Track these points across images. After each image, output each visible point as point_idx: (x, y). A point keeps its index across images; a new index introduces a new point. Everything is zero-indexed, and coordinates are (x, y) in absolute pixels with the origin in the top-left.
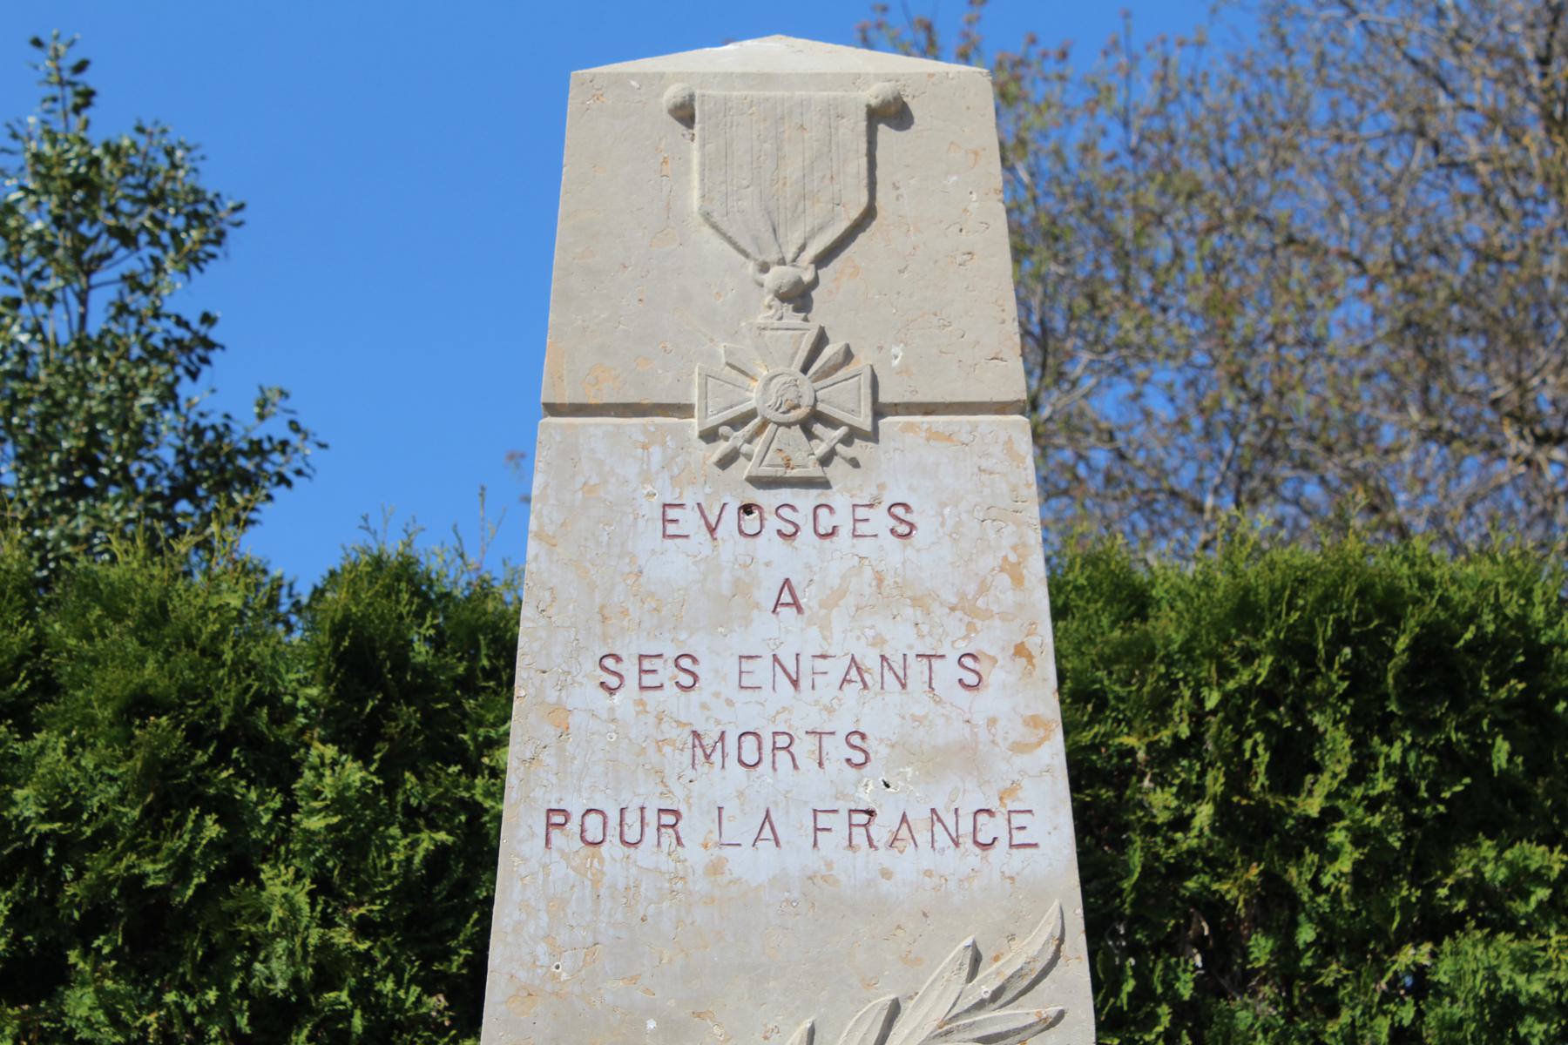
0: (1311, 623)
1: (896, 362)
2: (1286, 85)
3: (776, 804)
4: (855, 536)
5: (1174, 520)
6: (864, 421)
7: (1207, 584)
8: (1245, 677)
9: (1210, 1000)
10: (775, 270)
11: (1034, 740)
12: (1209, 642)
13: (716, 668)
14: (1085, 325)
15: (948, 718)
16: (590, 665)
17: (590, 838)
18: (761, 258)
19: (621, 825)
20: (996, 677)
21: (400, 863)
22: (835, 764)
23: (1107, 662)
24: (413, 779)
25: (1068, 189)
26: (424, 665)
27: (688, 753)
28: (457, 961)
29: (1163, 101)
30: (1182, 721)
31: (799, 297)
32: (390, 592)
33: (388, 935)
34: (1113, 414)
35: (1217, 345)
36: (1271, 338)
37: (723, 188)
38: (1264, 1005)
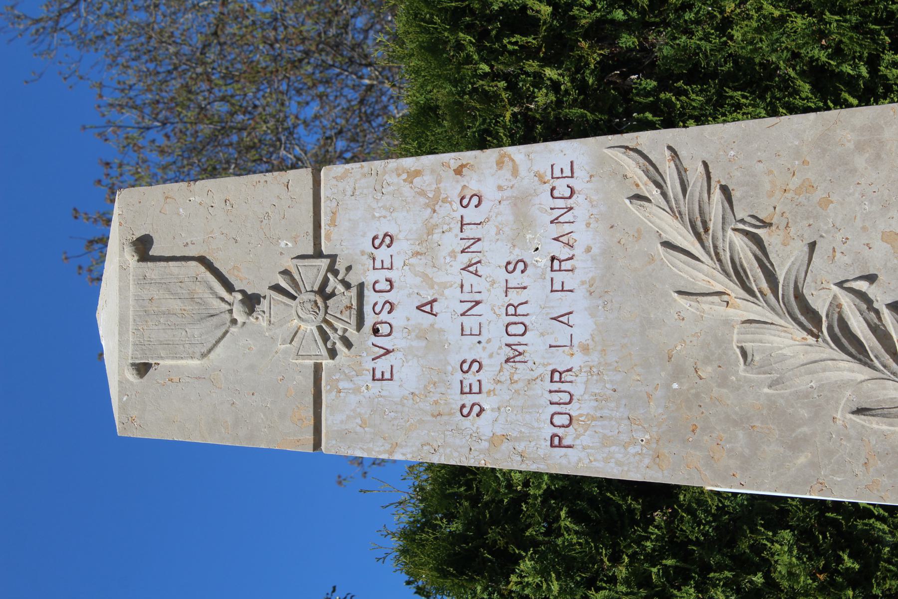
0: (440, 10)
1: (290, 245)
2: (123, 35)
3: (548, 314)
4: (391, 269)
5: (377, 102)
6: (324, 263)
7: (417, 72)
8: (471, 49)
9: (657, 70)
10: (235, 316)
11: (510, 164)
12: (451, 69)
13: (468, 350)
14: (264, 152)
15: (497, 214)
16: (466, 423)
17: (567, 422)
18: (228, 324)
19: (560, 404)
20: (474, 186)
21: (578, 538)
22: (524, 280)
23: (463, 129)
24: (530, 530)
25: (185, 162)
26: (464, 524)
27: (518, 365)
28: (635, 505)
29: (135, 107)
30: (496, 86)
31: (251, 302)
32: (421, 544)
33: (619, 544)
34: (316, 137)
35: (276, 76)
36: (272, 45)
37: (186, 346)
38: (660, 39)
